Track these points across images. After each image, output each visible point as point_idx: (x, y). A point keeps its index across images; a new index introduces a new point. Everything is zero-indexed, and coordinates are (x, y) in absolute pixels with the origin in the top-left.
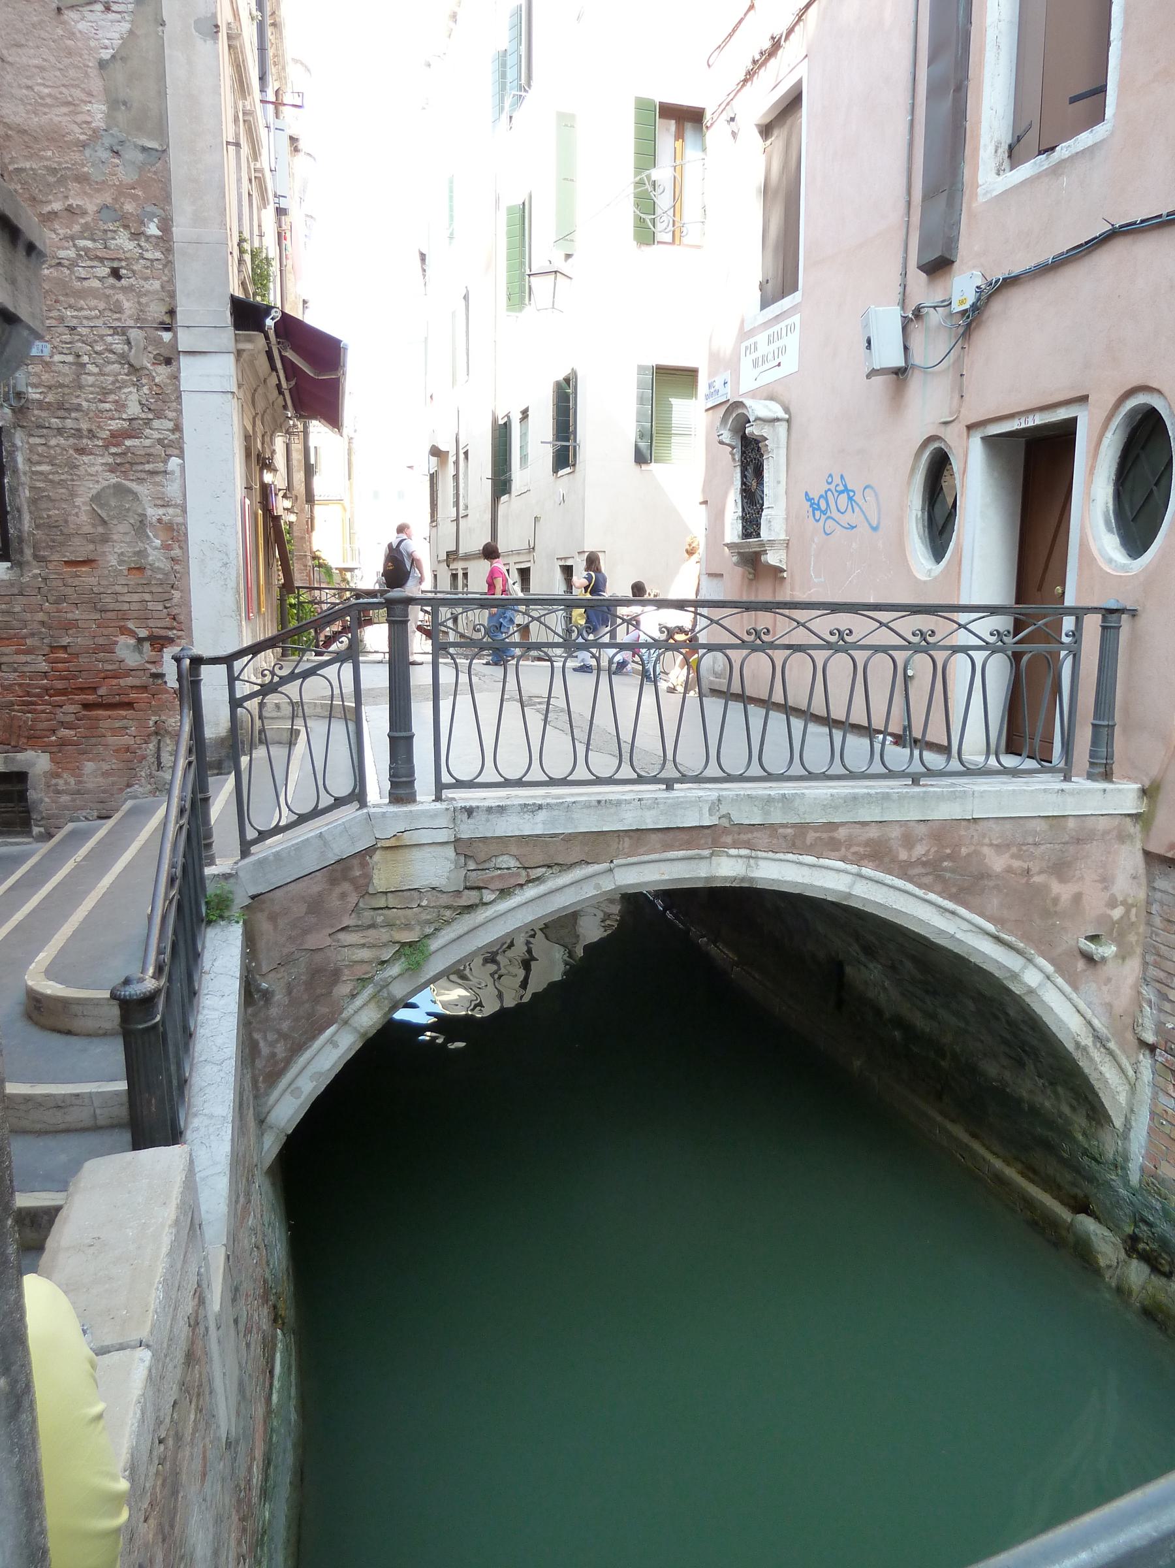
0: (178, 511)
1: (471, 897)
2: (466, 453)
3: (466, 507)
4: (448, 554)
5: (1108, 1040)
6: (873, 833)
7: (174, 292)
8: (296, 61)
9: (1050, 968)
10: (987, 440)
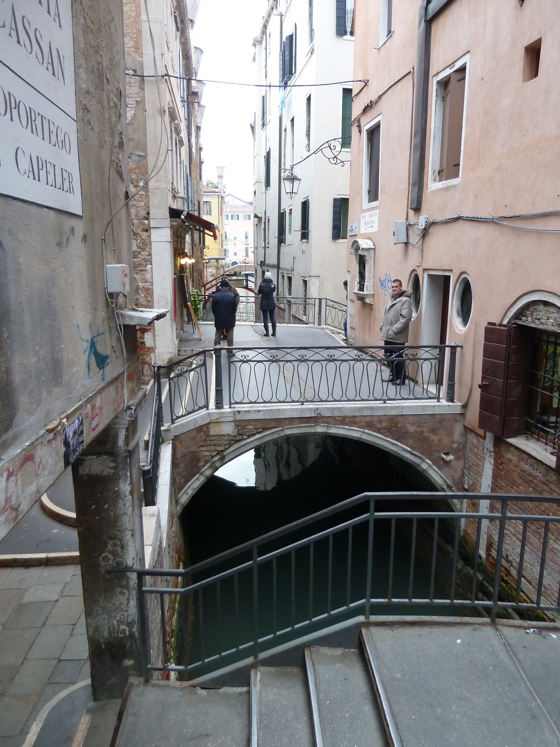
0: (150, 284)
1: (240, 437)
2: (269, 220)
3: (268, 244)
4: (261, 262)
5: (452, 487)
6: (368, 419)
7: (149, 206)
8: (196, 48)
9: (430, 463)
10: (429, 275)
